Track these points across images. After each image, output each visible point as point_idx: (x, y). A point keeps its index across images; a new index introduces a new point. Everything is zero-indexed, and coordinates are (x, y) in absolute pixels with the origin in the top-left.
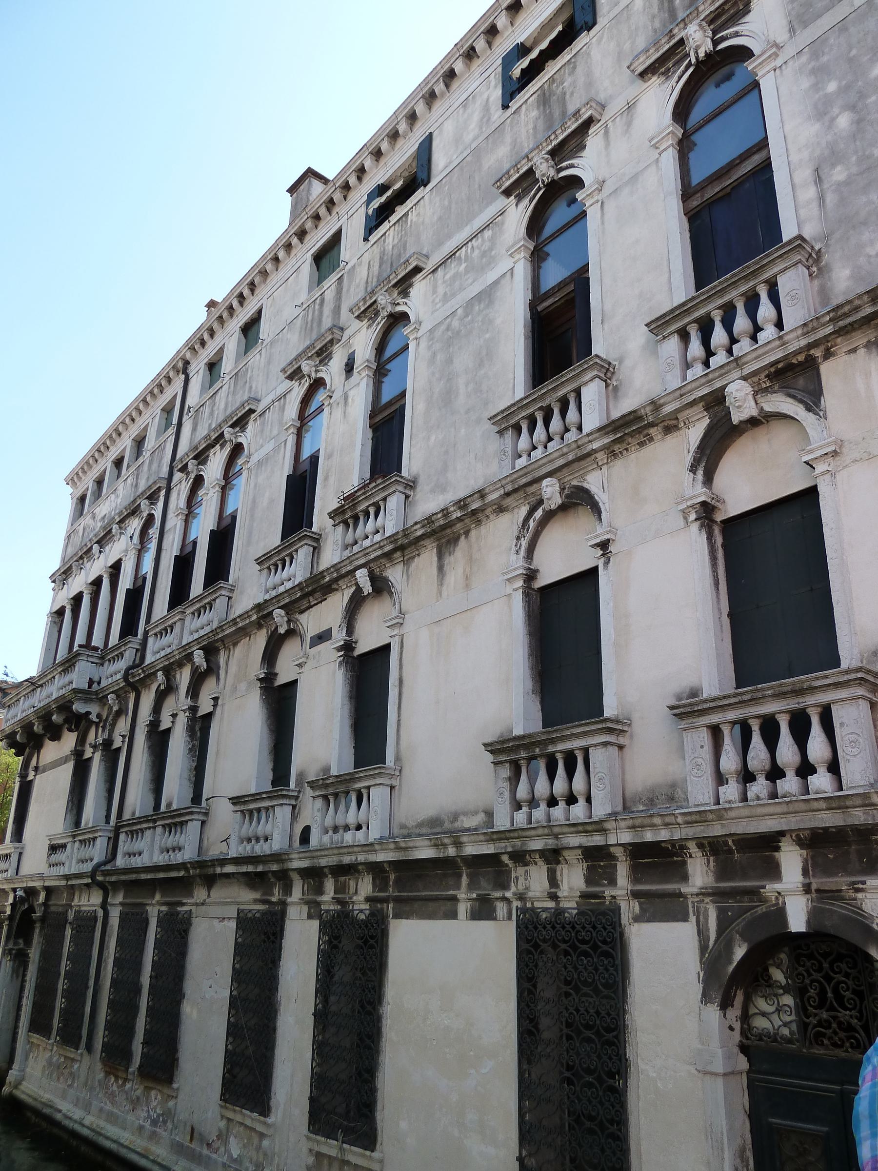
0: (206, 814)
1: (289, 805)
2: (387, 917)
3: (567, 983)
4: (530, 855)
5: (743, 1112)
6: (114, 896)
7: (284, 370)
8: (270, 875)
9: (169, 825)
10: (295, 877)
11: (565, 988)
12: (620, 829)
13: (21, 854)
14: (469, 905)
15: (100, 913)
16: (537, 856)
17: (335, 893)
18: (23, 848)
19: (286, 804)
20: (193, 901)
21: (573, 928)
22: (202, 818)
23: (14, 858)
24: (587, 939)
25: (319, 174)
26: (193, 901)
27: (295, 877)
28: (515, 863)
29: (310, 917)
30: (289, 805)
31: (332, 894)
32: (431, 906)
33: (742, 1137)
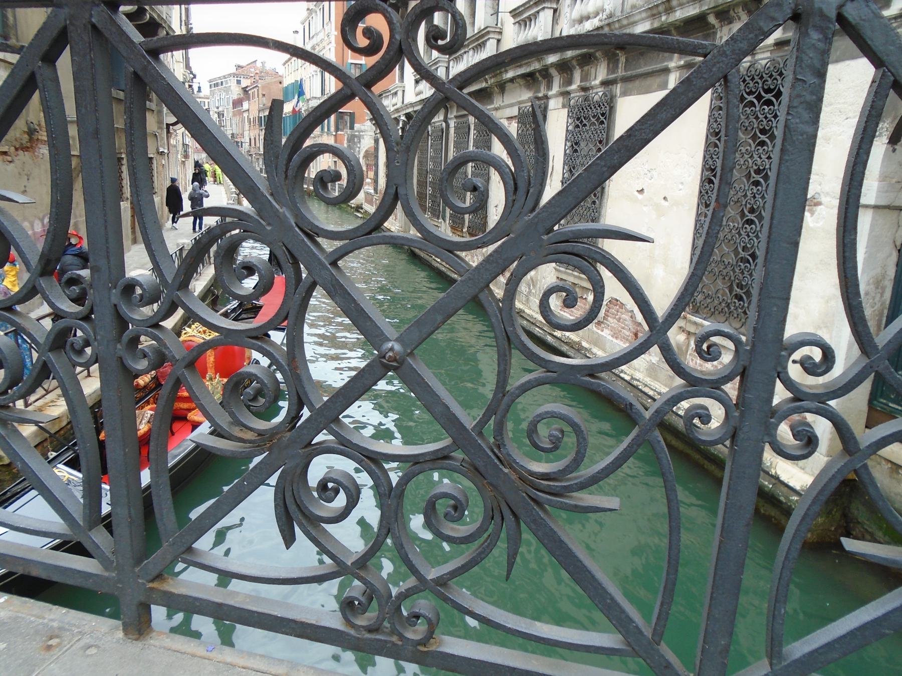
0: (500, 33)
1: (551, 8)
2: (616, 96)
3: (578, 119)
4: (734, 10)
5: (892, 246)
6: (451, 113)
7: (210, 81)
8: (537, 74)
9: (476, 47)
10: (553, 72)
11: (578, 123)
12: (497, 25)
13: (404, 91)
14: (678, 74)
15: (444, 124)
16: (740, 10)
17: (581, 82)
18: (404, 87)
19: (548, 8)
20: (492, 106)
21: (762, 77)
22: (497, 37)
23: (400, 94)
24: (772, 87)
25: (49, 503)
26: (492, 106)
27: (553, 72)
28: (720, 22)
29: (564, 106)
30: (551, 8)
31: (578, 83)
32: (649, 81)
33: (884, 267)
